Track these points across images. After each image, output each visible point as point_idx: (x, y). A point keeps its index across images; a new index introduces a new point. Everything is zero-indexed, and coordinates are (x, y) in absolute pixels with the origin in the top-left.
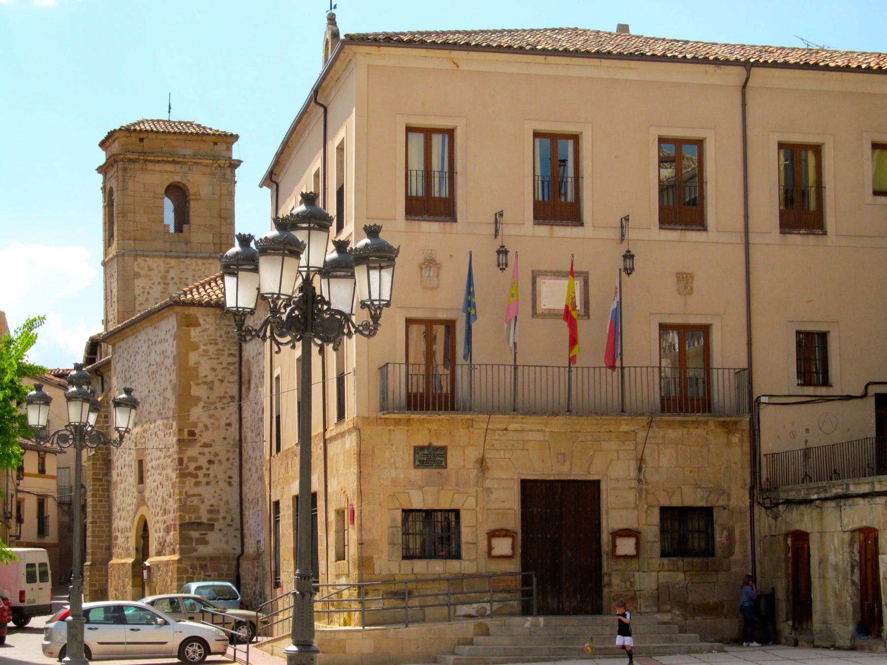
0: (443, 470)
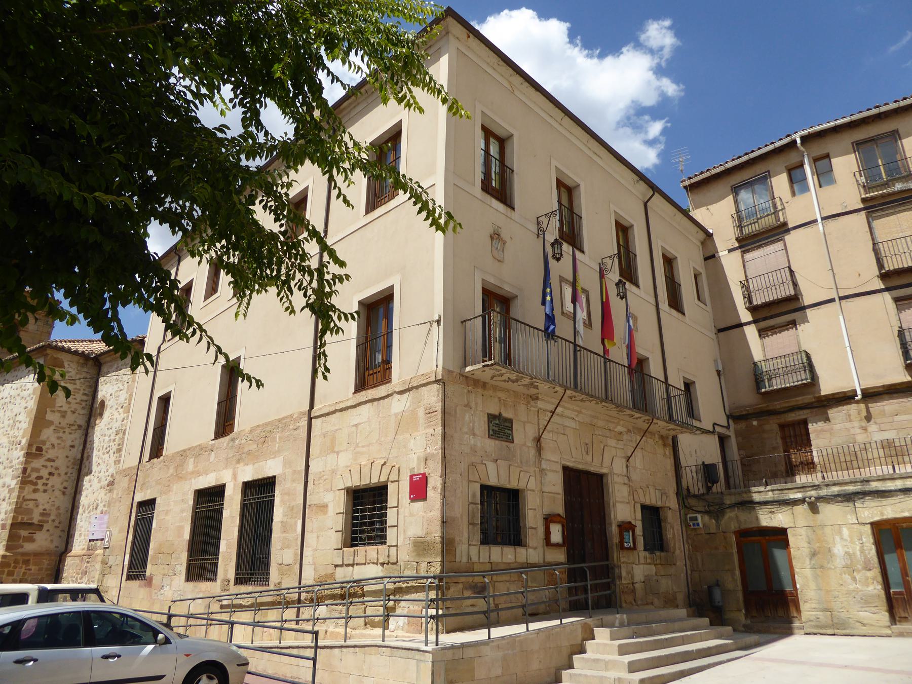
0: (511, 445)
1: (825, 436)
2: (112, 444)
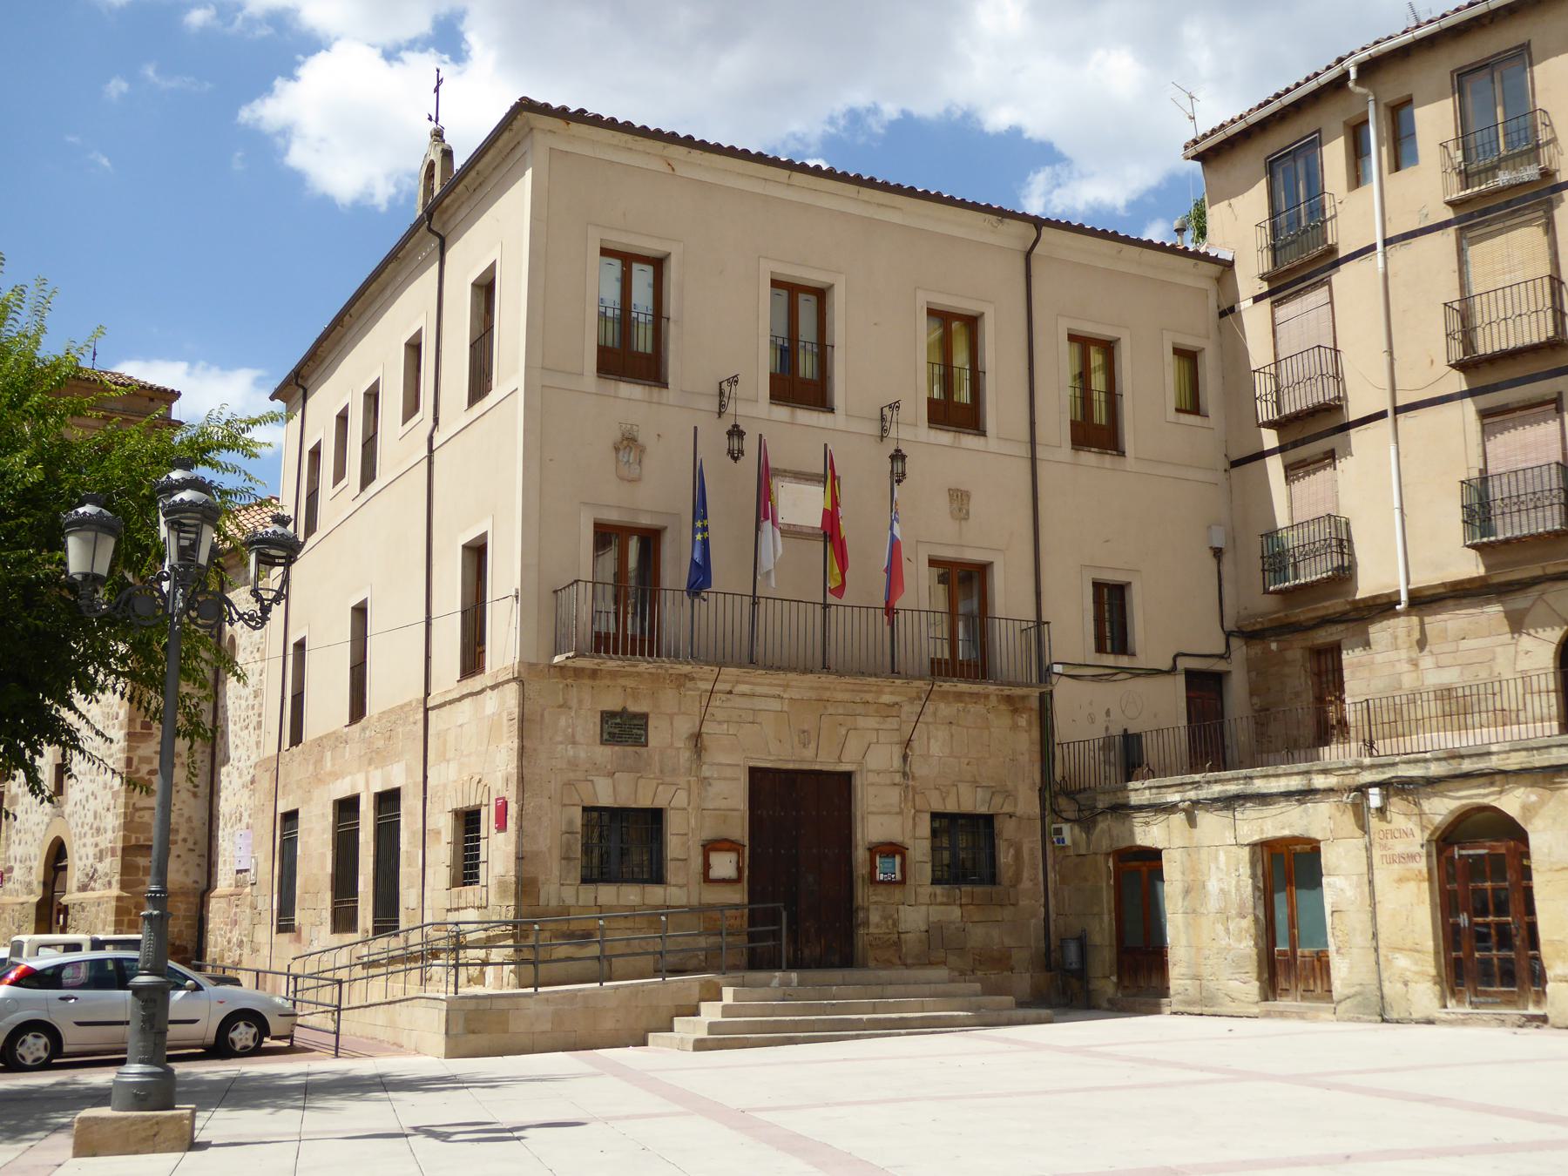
0: (643, 750)
1: (1375, 669)
2: (250, 713)
